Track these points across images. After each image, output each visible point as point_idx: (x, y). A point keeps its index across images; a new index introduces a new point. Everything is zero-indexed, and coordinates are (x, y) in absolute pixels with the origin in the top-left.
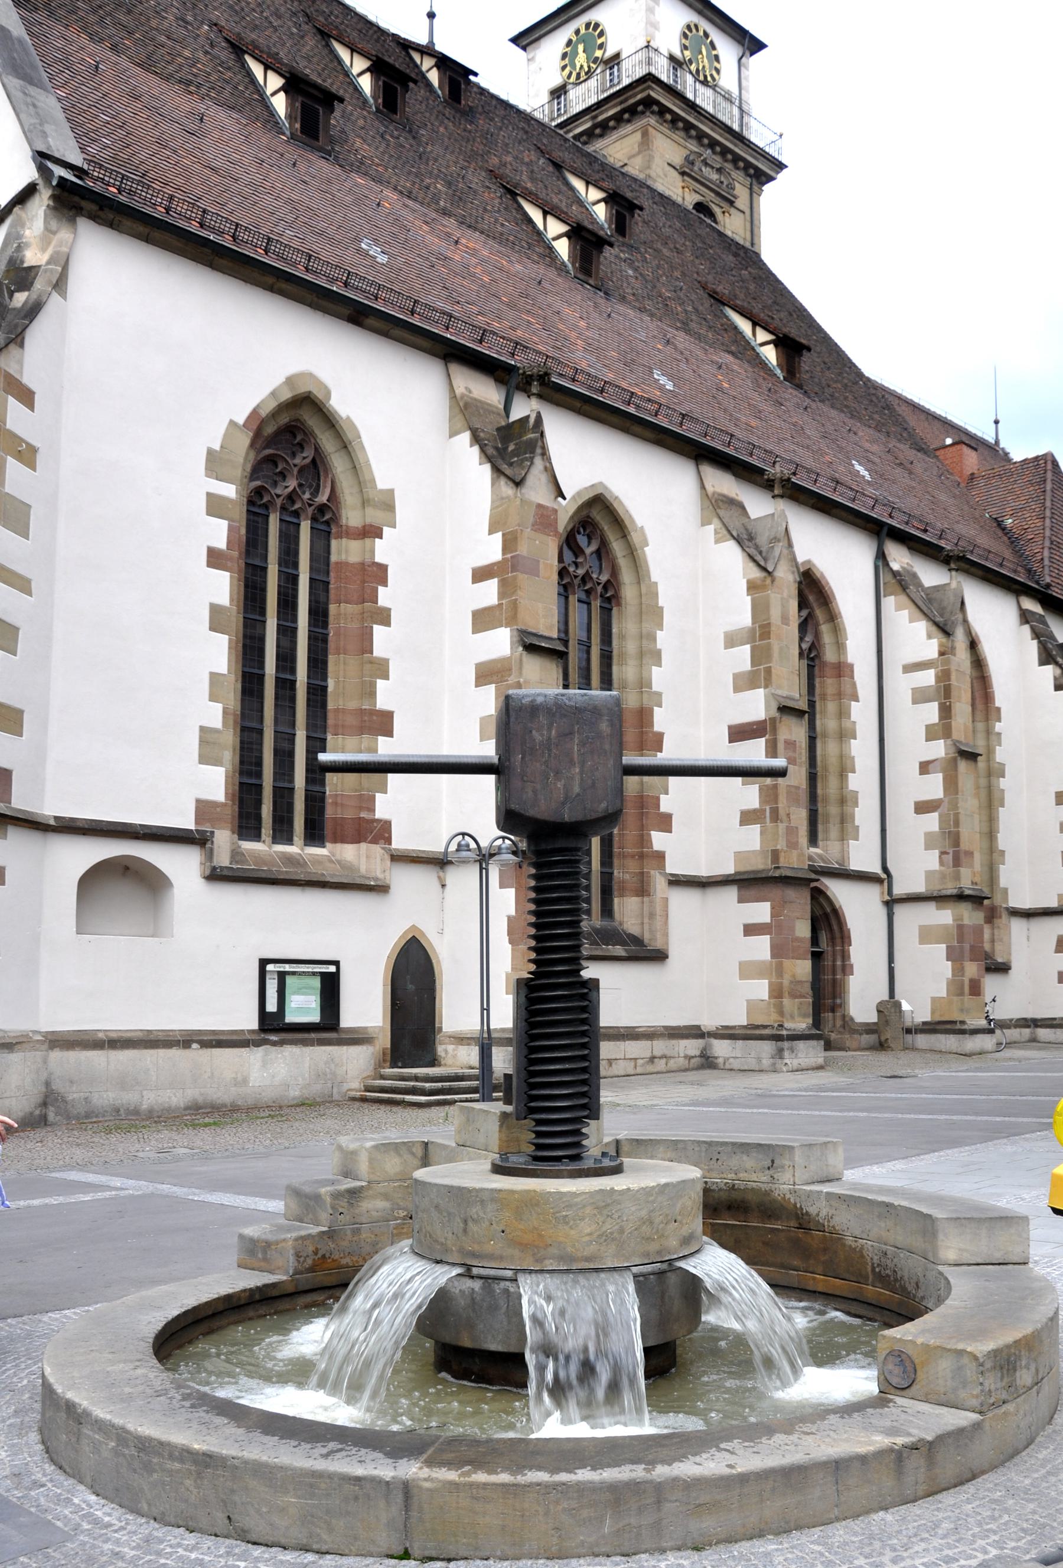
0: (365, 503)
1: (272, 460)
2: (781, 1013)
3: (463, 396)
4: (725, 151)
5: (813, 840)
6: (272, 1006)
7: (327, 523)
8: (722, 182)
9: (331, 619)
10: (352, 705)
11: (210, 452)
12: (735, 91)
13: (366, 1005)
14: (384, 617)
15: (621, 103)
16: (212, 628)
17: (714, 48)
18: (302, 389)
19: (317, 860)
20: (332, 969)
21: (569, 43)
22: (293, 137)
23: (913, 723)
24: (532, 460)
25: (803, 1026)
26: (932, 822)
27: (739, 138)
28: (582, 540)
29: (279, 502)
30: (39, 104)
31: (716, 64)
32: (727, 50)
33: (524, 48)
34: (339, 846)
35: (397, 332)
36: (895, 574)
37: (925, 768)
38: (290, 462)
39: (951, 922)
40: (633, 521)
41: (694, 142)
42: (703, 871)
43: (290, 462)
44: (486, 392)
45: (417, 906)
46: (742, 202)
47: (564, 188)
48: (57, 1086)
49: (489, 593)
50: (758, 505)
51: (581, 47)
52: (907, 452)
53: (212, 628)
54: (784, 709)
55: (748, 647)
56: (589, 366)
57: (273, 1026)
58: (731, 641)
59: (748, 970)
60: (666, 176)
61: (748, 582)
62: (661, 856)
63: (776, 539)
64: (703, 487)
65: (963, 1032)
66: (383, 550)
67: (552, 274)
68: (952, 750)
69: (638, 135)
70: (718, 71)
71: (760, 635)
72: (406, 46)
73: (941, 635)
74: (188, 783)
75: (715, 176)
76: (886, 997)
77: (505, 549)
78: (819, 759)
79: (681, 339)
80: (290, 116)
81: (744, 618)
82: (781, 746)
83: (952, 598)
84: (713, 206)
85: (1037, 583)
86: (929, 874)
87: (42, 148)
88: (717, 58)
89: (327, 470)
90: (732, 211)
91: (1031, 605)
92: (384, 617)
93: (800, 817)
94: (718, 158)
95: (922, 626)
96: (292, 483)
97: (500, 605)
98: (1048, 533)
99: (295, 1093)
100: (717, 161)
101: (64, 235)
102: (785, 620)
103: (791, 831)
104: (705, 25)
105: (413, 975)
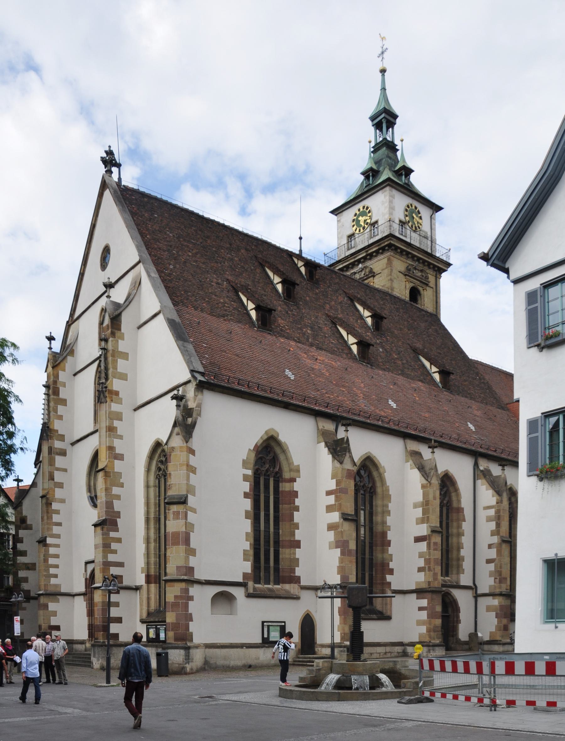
1: (261, 458)
2: (430, 637)
3: (322, 429)
4: (424, 262)
6: (266, 636)
7: (278, 478)
8: (423, 276)
10: (287, 539)
11: (243, 460)
12: (429, 234)
14: (297, 509)
15: (378, 245)
17: (419, 213)
19: (278, 590)
20: (283, 624)
21: (356, 215)
23: (486, 528)
24: (345, 454)
25: (438, 642)
26: (492, 567)
28: (362, 472)
29: (263, 473)
30: (188, 349)
32: (425, 212)
33: (336, 215)
36: (482, 471)
38: (268, 461)
40: (380, 464)
41: (411, 260)
42: (405, 588)
43: (268, 461)
44: (329, 426)
45: (307, 603)
46: (432, 284)
47: (355, 311)
48: (208, 659)
49: (331, 500)
50: (425, 452)
52: (495, 410)
54: (433, 531)
55: (421, 508)
56: (365, 406)
58: (415, 506)
59: (420, 623)
60: (398, 277)
61: (422, 485)
62: (389, 584)
63: (431, 469)
64: (406, 448)
65: (500, 644)
66: (297, 486)
67: (350, 363)
69: (386, 259)
71: (425, 504)
72: (290, 254)
73: (497, 496)
74: (238, 567)
75: (419, 274)
77: (337, 485)
79: (401, 380)
80: (257, 319)
81: (420, 498)
82: (432, 544)
84: (419, 287)
86: (490, 586)
87: (192, 369)
90: (428, 288)
92: (297, 509)
94: (421, 265)
95: (491, 492)
96: (267, 466)
97: (335, 504)
100: (421, 267)
101: (200, 396)
102: (435, 498)
103: (435, 575)
104: (415, 203)
105: (308, 625)
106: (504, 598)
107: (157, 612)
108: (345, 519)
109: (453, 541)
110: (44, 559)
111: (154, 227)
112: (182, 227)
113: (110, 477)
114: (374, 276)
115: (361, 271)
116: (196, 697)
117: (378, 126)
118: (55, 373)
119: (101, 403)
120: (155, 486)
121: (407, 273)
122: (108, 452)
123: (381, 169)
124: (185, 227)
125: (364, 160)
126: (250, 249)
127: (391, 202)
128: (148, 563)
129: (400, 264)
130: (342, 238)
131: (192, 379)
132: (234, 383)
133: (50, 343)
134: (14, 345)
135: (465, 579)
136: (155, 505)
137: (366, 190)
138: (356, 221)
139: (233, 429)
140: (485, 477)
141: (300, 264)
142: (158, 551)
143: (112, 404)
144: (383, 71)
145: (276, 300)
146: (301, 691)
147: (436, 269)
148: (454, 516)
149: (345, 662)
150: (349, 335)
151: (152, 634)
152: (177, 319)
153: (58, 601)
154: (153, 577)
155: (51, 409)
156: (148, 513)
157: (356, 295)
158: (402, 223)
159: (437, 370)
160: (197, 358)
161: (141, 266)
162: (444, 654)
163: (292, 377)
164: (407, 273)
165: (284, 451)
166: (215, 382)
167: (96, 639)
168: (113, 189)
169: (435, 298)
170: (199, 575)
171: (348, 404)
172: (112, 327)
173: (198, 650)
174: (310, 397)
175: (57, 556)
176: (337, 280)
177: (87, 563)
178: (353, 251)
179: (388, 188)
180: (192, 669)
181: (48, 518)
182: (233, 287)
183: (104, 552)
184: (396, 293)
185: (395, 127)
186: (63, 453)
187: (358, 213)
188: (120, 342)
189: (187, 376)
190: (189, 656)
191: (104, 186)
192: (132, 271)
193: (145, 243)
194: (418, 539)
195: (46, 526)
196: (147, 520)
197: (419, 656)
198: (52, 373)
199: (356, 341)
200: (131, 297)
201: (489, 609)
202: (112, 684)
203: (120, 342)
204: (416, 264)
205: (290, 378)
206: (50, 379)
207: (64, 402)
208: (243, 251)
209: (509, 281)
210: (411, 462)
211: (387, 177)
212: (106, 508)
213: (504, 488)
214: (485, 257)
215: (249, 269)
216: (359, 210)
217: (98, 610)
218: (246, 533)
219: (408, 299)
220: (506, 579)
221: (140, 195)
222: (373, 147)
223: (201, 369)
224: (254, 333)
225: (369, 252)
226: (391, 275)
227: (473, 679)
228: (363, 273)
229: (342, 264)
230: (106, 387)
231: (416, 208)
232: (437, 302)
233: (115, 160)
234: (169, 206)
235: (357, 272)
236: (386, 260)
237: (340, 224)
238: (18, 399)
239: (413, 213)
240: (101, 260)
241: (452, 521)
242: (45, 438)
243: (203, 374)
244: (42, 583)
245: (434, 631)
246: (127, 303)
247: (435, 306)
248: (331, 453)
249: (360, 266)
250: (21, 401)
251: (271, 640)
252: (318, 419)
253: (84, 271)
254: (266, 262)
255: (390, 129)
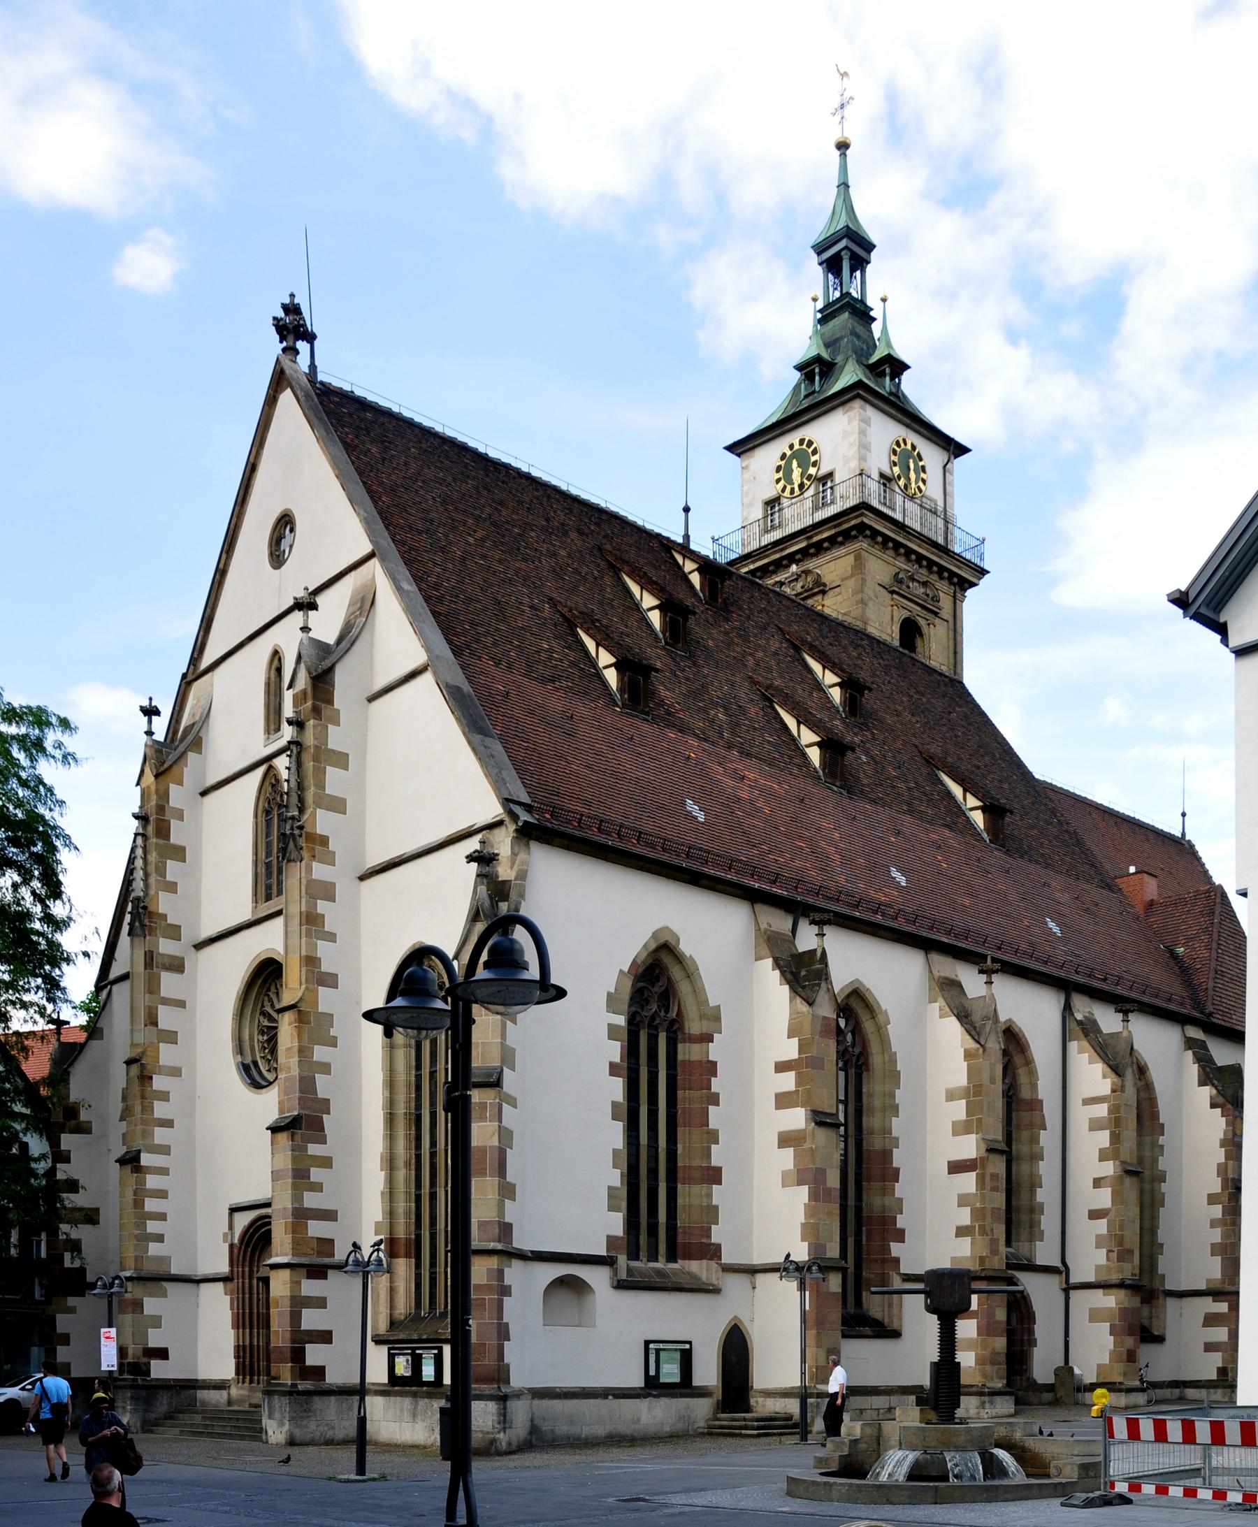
0: (702, 1017)
2: (984, 1376)
4: (931, 563)
5: (1008, 1243)
6: (652, 1372)
9: (679, 1101)
11: (609, 994)
12: (940, 503)
13: (707, 1372)
14: (715, 1099)
15: (835, 526)
16: (613, 1119)
17: (921, 459)
18: (662, 941)
20: (687, 1346)
21: (783, 456)
22: (624, 706)
24: (819, 985)
26: (1102, 1226)
27: (945, 550)
29: (647, 1021)
31: (922, 475)
32: (932, 456)
33: (739, 455)
34: (687, 1262)
35: (719, 887)
36: (1080, 1023)
37: (1097, 1183)
38: (657, 996)
39: (1114, 1305)
41: (903, 559)
43: (657, 996)
44: (780, 922)
46: (946, 612)
49: (788, 1081)
50: (972, 982)
51: (795, 463)
52: (1095, 893)
53: (613, 1119)
55: (964, 1101)
56: (847, 881)
57: (653, 1386)
58: (951, 1096)
61: (965, 1051)
63: (987, 1018)
65: (1120, 1391)
66: (715, 1051)
68: (1119, 1169)
69: (852, 557)
70: (924, 482)
71: (973, 1093)
73: (1113, 1075)
74: (595, 1223)
76: (1062, 1364)
78: (1014, 1177)
80: (621, 689)
82: (988, 1178)
83: (1124, 1046)
85: (1202, 1013)
86: (1098, 1268)
88: (923, 469)
89: (675, 994)
90: (937, 621)
91: (1194, 1033)
92: (715, 1099)
93: (1000, 1230)
94: (924, 571)
95: (1099, 1067)
98: (1213, 964)
99: (667, 1429)
100: (923, 574)
101: (522, 856)
102: (992, 1080)
103: (994, 1242)
104: (913, 438)
105: (736, 1349)
106: (1129, 1292)
107: (412, 1320)
108: (820, 1124)
109: (1023, 1169)
110: (135, 1201)
111: (394, 477)
112: (449, 479)
113: (308, 1023)
114: (824, 592)
115: (796, 580)
116: (611, 1500)
117: (832, 266)
118: (162, 788)
119: (289, 861)
120: (408, 1046)
121: (896, 587)
122: (304, 969)
123: (839, 359)
124: (454, 480)
125: (798, 335)
126: (586, 531)
127: (862, 433)
128: (391, 1214)
129: (880, 567)
130: (751, 504)
131: (507, 819)
132: (570, 822)
133: (150, 722)
134: (65, 724)
135: (1045, 1253)
136: (408, 1086)
137: (805, 404)
138: (784, 470)
139: (593, 919)
140: (1086, 1035)
141: (689, 566)
142: (413, 1185)
143: (314, 863)
144: (843, 146)
145: (649, 646)
146: (850, 1485)
147: (956, 580)
148: (1023, 1117)
149: (917, 1424)
150: (802, 726)
151: (403, 1366)
152: (466, 687)
153: (164, 1294)
154: (403, 1242)
155: (152, 868)
156: (391, 1103)
157: (803, 635)
158: (886, 480)
159: (979, 803)
160: (514, 772)
161: (375, 564)
162: (1012, 1411)
163: (701, 817)
164: (896, 587)
165: (690, 973)
166: (554, 824)
167: (274, 1378)
168: (302, 389)
169: (951, 642)
170: (521, 1241)
171: (814, 876)
172: (315, 697)
173: (520, 1403)
174: (739, 861)
175: (162, 1194)
176: (763, 604)
177: (233, 1210)
178: (777, 535)
179: (857, 404)
180: (509, 1444)
181: (143, 1109)
182: (563, 615)
183: (295, 1187)
184: (873, 630)
185: (869, 268)
186: (177, 966)
187: (789, 453)
188: (331, 728)
189: (492, 809)
190: (505, 1416)
191: (279, 380)
192: (353, 573)
193: (380, 514)
194: (957, 1167)
195: (139, 1127)
196: (390, 1119)
197: (1102, 1411)
198: (153, 788)
199: (818, 739)
200: (355, 631)
201: (1095, 1316)
202: (369, 1475)
203: (331, 728)
204: (912, 568)
205: (696, 818)
206: (149, 800)
207: (179, 853)
208: (574, 535)
209: (1227, 650)
210: (941, 1002)
211: (854, 379)
212: (301, 1092)
213: (1128, 1060)
214: (1180, 600)
215: (590, 578)
216: (791, 447)
217: (280, 1314)
218: (614, 1150)
219: (896, 643)
220: (1131, 1252)
221: (358, 406)
222: (820, 311)
223: (525, 798)
224: (617, 718)
225: (815, 539)
226: (862, 592)
227: (1188, 1457)
228: (800, 584)
229: (753, 562)
230: (301, 828)
231: (914, 447)
232: (955, 653)
233: (304, 325)
234: (417, 430)
235: (788, 581)
236: (851, 558)
237: (747, 476)
238: (68, 842)
239: (909, 457)
240: (270, 545)
241: (1019, 1128)
242: (139, 931)
243: (528, 808)
244: (130, 1254)
245: (993, 1363)
246: (344, 645)
247: (952, 661)
248: (788, 983)
249: (794, 568)
250: (76, 848)
251: (662, 1380)
252: (758, 907)
253: (227, 564)
254: (624, 562)
255: (858, 273)
